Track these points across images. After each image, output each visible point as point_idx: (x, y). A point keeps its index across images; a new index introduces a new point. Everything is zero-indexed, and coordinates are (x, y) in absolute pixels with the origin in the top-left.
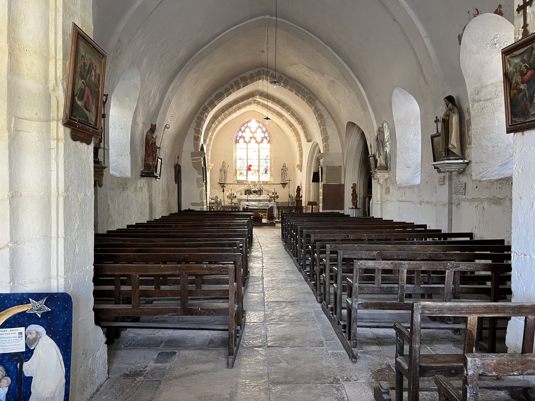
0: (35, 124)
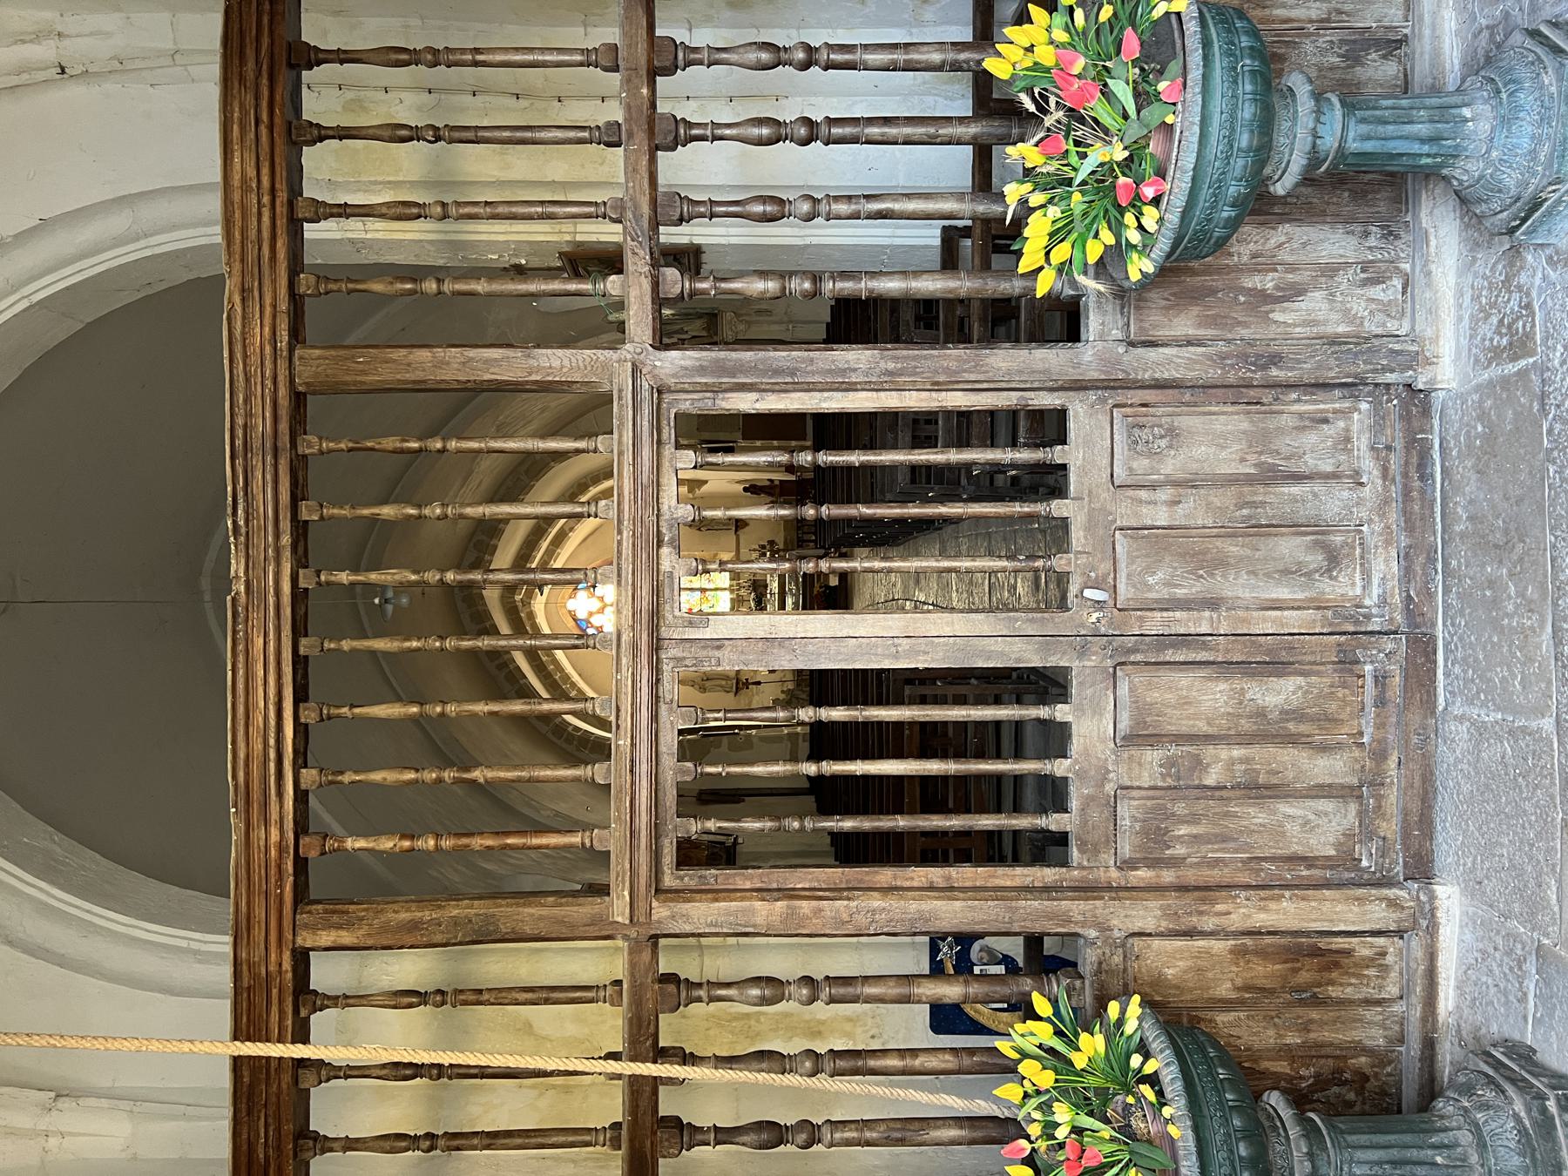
0: (707, 961)
